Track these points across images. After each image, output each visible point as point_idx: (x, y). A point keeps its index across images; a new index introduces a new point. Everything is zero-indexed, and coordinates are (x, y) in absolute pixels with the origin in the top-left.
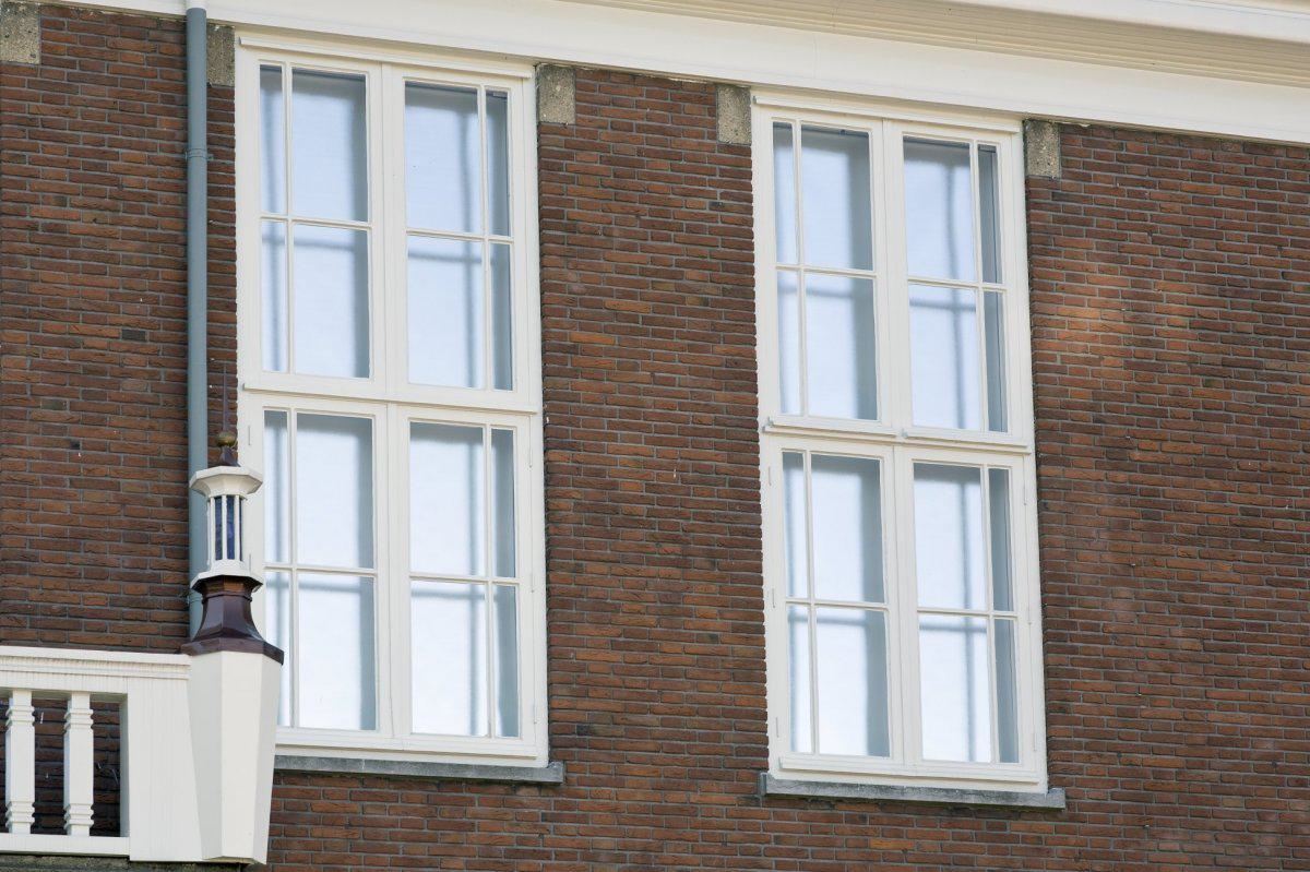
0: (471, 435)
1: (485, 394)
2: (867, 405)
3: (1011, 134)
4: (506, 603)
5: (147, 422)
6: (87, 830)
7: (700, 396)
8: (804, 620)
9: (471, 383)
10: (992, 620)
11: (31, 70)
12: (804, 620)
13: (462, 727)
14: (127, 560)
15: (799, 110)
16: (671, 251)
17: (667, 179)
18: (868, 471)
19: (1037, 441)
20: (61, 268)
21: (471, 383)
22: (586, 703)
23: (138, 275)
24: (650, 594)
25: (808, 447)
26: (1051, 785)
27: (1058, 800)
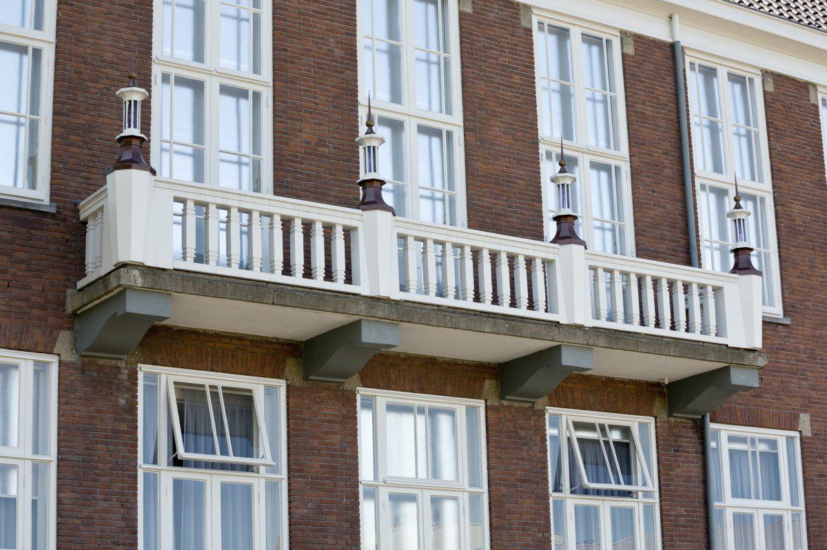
0: (22, 50)
1: (29, 30)
2: (199, 55)
3: (617, 36)
4: (34, 127)
5: (672, 185)
6: (490, 302)
7: (813, 191)
8: (167, 151)
9: (23, 25)
10: (28, 120)
11: (632, 57)
12: (167, 151)
13: (10, 183)
14: (670, 234)
15: (548, 18)
16: (802, 140)
17: (798, 114)
18: (197, 87)
19: (274, 81)
20: (646, 127)
21: (23, 25)
22: (793, 297)
23: (665, 132)
24: (806, 259)
25: (173, 72)
26: (785, 315)
27: (53, 210)
